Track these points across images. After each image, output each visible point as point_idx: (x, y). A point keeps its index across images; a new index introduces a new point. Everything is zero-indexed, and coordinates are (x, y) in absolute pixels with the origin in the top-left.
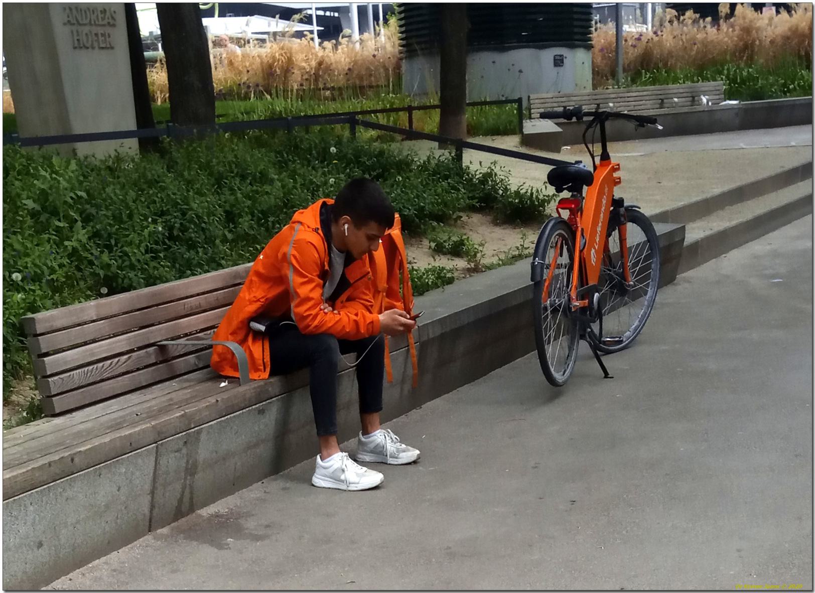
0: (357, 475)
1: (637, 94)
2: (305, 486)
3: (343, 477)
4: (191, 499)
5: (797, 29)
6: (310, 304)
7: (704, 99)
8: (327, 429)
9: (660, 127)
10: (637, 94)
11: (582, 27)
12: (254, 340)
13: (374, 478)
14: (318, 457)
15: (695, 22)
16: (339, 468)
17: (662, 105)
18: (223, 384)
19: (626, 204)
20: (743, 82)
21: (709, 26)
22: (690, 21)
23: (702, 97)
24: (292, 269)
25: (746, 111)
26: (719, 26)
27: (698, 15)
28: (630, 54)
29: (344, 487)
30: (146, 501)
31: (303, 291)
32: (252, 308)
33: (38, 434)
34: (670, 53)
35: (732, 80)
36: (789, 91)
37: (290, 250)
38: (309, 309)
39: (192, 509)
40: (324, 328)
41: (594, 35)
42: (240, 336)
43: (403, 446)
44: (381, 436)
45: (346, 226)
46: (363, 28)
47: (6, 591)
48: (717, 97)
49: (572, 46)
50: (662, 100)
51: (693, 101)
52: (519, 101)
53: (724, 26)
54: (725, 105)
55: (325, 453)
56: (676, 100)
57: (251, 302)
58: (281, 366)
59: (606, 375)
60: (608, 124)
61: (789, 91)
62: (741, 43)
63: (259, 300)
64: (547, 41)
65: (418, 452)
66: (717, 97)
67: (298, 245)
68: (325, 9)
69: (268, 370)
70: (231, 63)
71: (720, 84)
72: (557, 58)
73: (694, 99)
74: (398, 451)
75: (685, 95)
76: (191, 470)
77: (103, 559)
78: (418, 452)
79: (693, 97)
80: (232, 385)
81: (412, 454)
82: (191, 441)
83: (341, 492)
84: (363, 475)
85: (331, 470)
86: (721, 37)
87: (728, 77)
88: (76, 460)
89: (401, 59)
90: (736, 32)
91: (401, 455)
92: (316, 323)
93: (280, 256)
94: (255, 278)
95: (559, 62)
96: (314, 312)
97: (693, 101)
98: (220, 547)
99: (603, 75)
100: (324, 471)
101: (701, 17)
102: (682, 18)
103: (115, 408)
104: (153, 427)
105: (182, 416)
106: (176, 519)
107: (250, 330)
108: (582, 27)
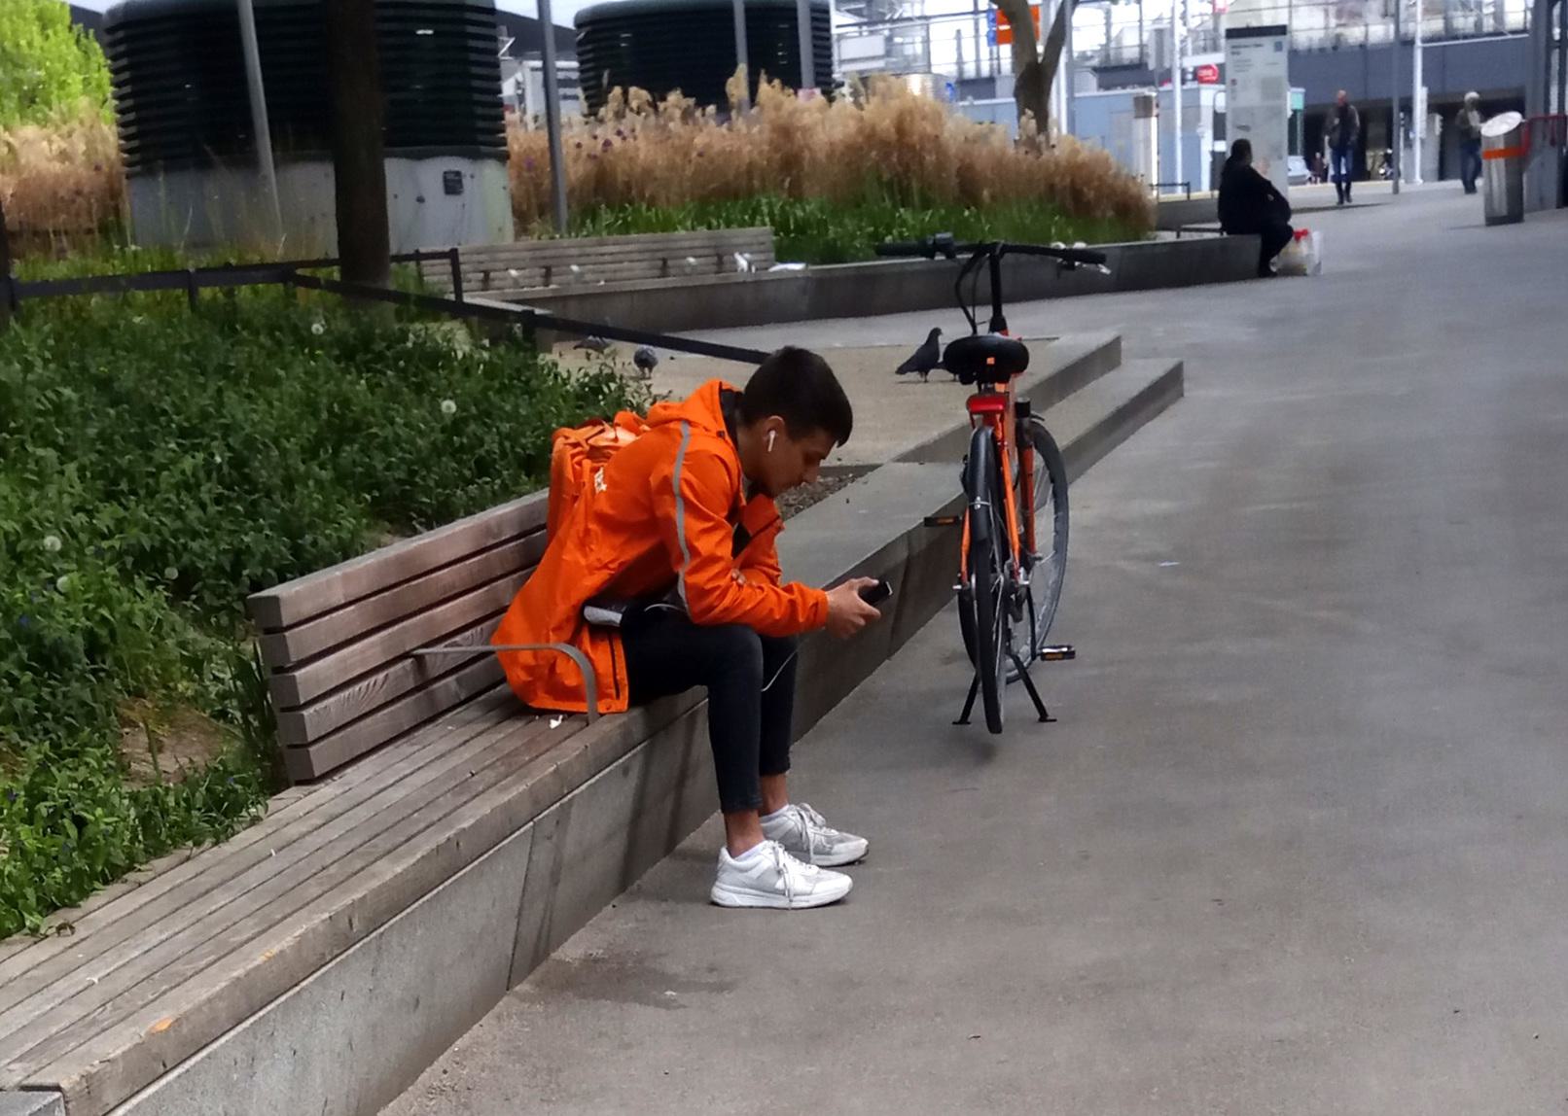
0: (807, 878)
1: (616, 249)
2: (699, 908)
3: (780, 885)
5: (873, 128)
6: (717, 568)
7: (742, 262)
10: (616, 249)
12: (593, 642)
15: (687, 115)
16: (786, 866)
17: (664, 271)
18: (554, 724)
21: (712, 123)
22: (678, 113)
23: (738, 256)
24: (680, 504)
25: (821, 283)
26: (729, 119)
27: (691, 101)
28: (574, 170)
29: (782, 902)
31: (705, 545)
32: (593, 581)
33: (331, 809)
34: (648, 172)
35: (781, 226)
37: (678, 472)
38: (717, 576)
39: (547, 954)
40: (739, 612)
41: (510, 134)
42: (567, 634)
43: (834, 832)
45: (773, 435)
48: (762, 257)
49: (475, 156)
50: (665, 261)
51: (720, 262)
52: (453, 255)
53: (740, 123)
54: (781, 272)
55: (738, 843)
56: (692, 260)
57: (592, 570)
58: (650, 685)
62: (778, 156)
63: (606, 567)
64: (430, 143)
65: (864, 842)
66: (762, 257)
67: (694, 460)
71: (763, 232)
72: (451, 177)
73: (721, 259)
74: (830, 840)
75: (706, 252)
78: (864, 842)
79: (720, 257)
80: (576, 725)
82: (562, 820)
84: (818, 880)
85: (754, 874)
87: (773, 222)
91: (838, 847)
92: (727, 602)
93: (654, 481)
94: (593, 526)
95: (453, 185)
96: (723, 582)
97: (720, 262)
98: (668, 1005)
99: (533, 207)
100: (741, 877)
102: (661, 106)
104: (531, 790)
106: (532, 968)
107: (580, 621)
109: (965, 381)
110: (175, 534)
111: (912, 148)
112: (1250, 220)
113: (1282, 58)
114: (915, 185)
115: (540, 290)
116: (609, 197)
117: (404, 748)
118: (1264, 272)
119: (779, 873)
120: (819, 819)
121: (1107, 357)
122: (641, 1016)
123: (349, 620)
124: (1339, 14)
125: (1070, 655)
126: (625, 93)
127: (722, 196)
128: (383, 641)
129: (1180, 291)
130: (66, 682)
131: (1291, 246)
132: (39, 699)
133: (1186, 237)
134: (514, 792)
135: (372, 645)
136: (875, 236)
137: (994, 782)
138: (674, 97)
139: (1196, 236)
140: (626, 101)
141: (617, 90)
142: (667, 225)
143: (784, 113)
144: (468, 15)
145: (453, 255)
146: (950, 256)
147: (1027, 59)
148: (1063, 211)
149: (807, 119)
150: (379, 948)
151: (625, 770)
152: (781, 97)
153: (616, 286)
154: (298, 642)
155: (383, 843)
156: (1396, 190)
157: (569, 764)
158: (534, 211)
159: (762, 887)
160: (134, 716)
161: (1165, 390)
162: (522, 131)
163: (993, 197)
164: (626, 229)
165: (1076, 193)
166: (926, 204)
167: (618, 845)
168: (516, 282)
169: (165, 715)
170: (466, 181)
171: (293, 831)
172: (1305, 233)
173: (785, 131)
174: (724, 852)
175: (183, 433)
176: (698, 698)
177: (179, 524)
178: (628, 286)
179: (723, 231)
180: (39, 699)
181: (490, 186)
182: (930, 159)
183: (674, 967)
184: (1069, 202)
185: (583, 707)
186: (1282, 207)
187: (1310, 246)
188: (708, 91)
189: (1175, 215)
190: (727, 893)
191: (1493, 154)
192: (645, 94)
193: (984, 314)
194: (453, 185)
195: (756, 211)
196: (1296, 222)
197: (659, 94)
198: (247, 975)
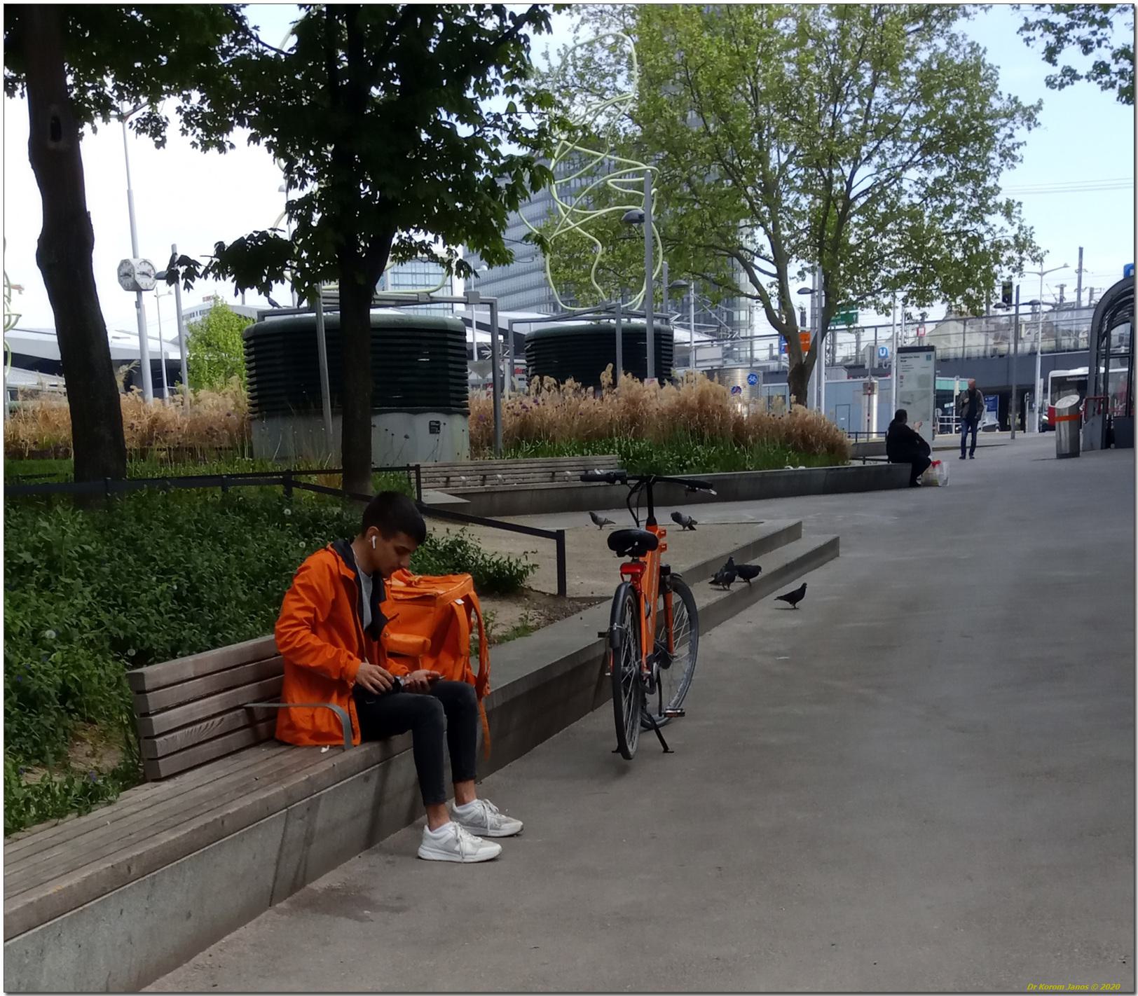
0: (473, 845)
3: (457, 848)
4: (305, 871)
8: (431, 797)
9: (713, 493)
11: (457, 392)
13: (493, 849)
14: (426, 828)
16: (463, 836)
17: (484, 479)
18: (324, 750)
19: (672, 571)
20: (636, 456)
27: (579, 385)
28: (508, 421)
29: (458, 859)
30: (271, 872)
33: (158, 798)
34: (552, 423)
36: (685, 467)
39: (303, 885)
44: (476, 807)
46: (157, 385)
47: (9, 993)
52: (417, 468)
55: (434, 823)
59: (666, 750)
60: (655, 489)
61: (685, 467)
65: (520, 823)
68: (5, 364)
69: (359, 736)
70: (46, 418)
74: (500, 822)
76: (308, 840)
77: (233, 935)
78: (520, 823)
80: (335, 752)
81: (514, 825)
82: (312, 808)
83: (455, 864)
85: (443, 841)
86: (604, 407)
88: (226, 823)
89: (252, 419)
90: (622, 404)
95: (434, 428)
98: (361, 919)
99: (483, 442)
101: (583, 386)
103: (221, 773)
104: (286, 790)
105: (307, 780)
106: (291, 894)
108: (457, 392)
109: (621, 554)
110: (140, 630)
111: (707, 412)
112: (906, 453)
113: (931, 363)
114: (707, 432)
115: (480, 489)
116: (529, 437)
117: (228, 761)
118: (913, 484)
119: (457, 841)
120: (494, 808)
121: (793, 533)
122: (346, 925)
123: (199, 685)
124: (996, 338)
125: (682, 714)
126: (541, 380)
127: (592, 437)
128: (220, 700)
129: (763, 502)
130: (38, 715)
131: (930, 470)
132: (20, 724)
133: (868, 463)
134: (273, 792)
135: (198, 707)
136: (680, 461)
137: (622, 787)
138: (569, 382)
139: (873, 463)
140: (542, 384)
141: (537, 377)
142: (561, 452)
143: (633, 391)
144: (449, 336)
145: (417, 468)
146: (624, 482)
147: (796, 361)
148: (795, 448)
149: (646, 395)
150: (153, 885)
151: (367, 778)
152: (632, 382)
153: (523, 487)
154: (153, 700)
155: (173, 821)
156: (1013, 437)
157: (319, 776)
158: (485, 443)
159: (447, 849)
160: (84, 734)
161: (828, 551)
162: (479, 398)
163: (754, 440)
164: (536, 454)
165: (804, 438)
166: (713, 442)
167: (364, 821)
168: (464, 483)
169: (103, 735)
170: (442, 426)
171: (127, 811)
172: (938, 462)
173: (633, 402)
174: (426, 828)
175: (164, 572)
176: (403, 741)
177: (145, 624)
178: (530, 486)
179: (590, 457)
180: (20, 724)
181: (457, 430)
182: (718, 418)
183: (377, 896)
184: (800, 445)
185: (343, 742)
186: (925, 448)
187: (942, 470)
188: (589, 379)
189: (867, 450)
190: (426, 852)
191: (1062, 419)
192: (553, 380)
193: (643, 515)
194: (434, 428)
195: (611, 446)
196: (932, 457)
197: (561, 380)
198: (40, 900)
